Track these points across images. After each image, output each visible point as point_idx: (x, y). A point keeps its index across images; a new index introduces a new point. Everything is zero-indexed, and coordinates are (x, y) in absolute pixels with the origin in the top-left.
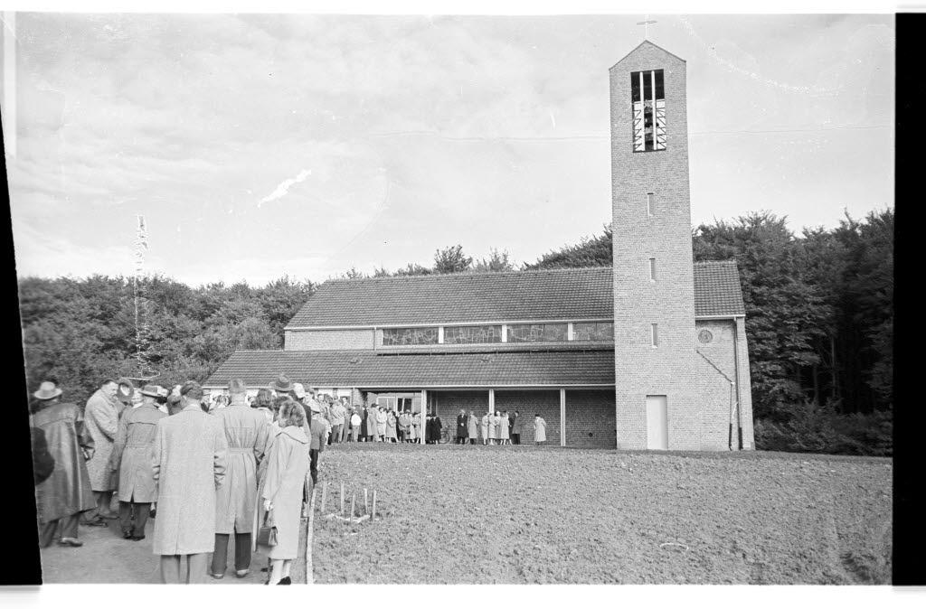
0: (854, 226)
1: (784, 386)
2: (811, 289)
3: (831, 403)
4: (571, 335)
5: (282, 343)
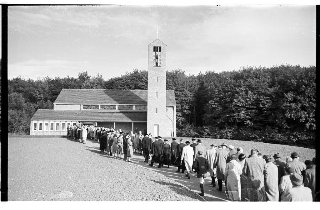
0: (202, 75)
1: (182, 119)
2: (190, 93)
3: (193, 124)
4: (134, 108)
5: (52, 108)
